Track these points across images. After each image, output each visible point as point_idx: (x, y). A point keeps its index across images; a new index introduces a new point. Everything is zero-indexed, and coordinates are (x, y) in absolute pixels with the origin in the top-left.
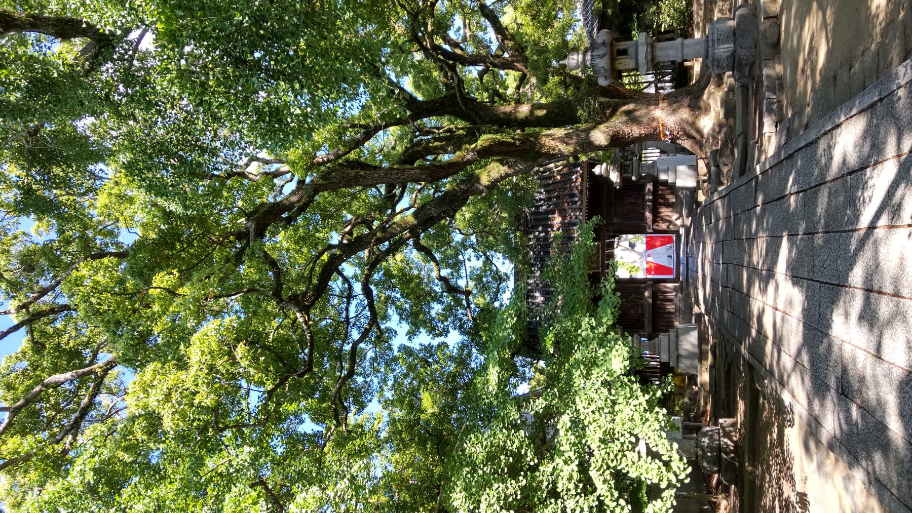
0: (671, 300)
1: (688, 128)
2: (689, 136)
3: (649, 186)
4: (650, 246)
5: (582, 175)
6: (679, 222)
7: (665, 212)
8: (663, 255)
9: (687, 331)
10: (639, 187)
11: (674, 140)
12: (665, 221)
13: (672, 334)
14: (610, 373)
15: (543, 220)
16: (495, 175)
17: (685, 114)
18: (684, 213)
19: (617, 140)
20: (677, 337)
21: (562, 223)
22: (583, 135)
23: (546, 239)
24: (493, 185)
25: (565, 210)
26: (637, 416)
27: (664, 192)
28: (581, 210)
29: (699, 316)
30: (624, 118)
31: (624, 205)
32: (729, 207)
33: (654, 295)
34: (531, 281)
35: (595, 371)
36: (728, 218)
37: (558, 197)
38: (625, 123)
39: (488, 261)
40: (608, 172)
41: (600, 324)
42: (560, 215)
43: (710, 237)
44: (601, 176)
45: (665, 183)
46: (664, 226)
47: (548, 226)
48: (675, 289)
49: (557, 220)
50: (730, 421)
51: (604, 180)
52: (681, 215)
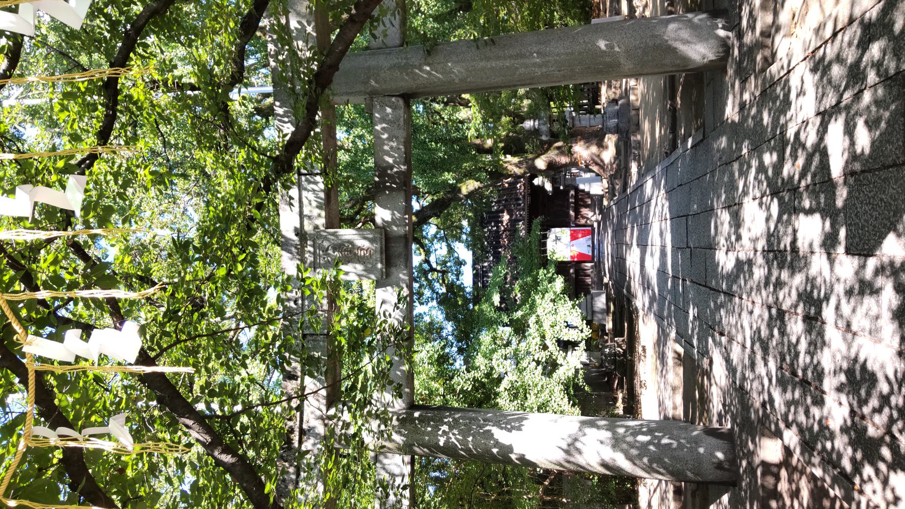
0: (589, 276)
1: (596, 159)
2: (597, 164)
3: (572, 192)
4: (574, 237)
5: (524, 185)
6: (593, 219)
7: (585, 211)
8: (582, 246)
9: (599, 295)
10: (566, 192)
11: (587, 166)
12: (583, 217)
13: (589, 297)
14: (555, 293)
15: (495, 218)
16: (471, 188)
17: (594, 149)
18: (597, 212)
19: (551, 166)
20: (592, 299)
21: (510, 220)
22: (530, 162)
23: (497, 231)
24: (471, 195)
25: (512, 210)
26: (567, 312)
27: (582, 199)
28: (524, 210)
29: (607, 284)
30: (557, 152)
31: (557, 206)
32: (618, 210)
33: (576, 272)
34: (486, 264)
35: (547, 295)
36: (618, 217)
37: (506, 200)
38: (557, 155)
39: (451, 250)
40: (543, 183)
41: (548, 272)
42: (508, 213)
43: (785, 246)
44: (538, 186)
45: (583, 191)
46: (583, 222)
47: (499, 222)
48: (592, 267)
49: (506, 217)
50: (621, 339)
51: (541, 188)
52: (595, 213)
